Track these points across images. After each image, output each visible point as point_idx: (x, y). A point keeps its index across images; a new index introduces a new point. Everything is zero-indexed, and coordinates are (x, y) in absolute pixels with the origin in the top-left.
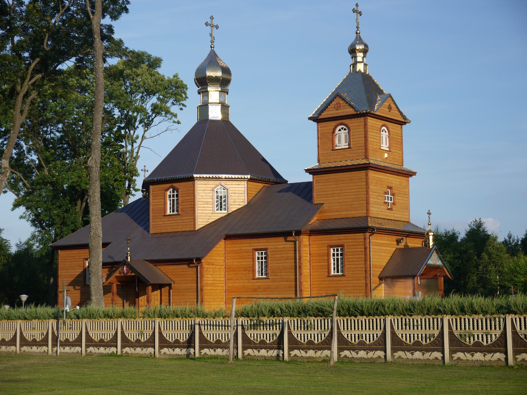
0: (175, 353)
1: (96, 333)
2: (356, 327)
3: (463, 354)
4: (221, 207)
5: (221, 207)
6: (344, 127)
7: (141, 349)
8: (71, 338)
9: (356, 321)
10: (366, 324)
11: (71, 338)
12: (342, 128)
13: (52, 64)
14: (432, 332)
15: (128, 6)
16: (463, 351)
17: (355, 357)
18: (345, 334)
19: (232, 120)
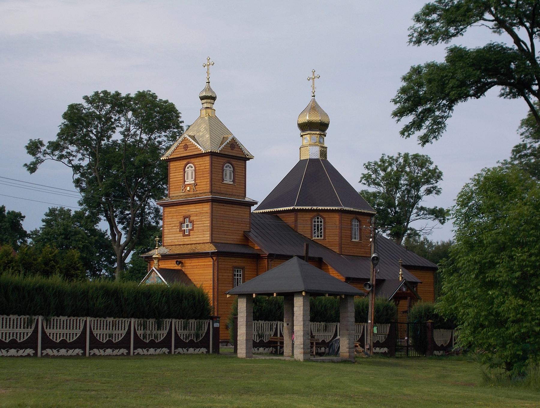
0: (149, 353)
1: (99, 330)
2: (68, 327)
3: (141, 350)
4: (318, 228)
5: (318, 228)
6: (231, 166)
7: (263, 349)
8: (101, 338)
9: (8, 320)
10: (17, 323)
11: (101, 338)
12: (228, 166)
13: (425, 93)
14: (75, 331)
15: (503, 97)
16: (51, 348)
17: (66, 355)
18: (95, 332)
19: (330, 159)
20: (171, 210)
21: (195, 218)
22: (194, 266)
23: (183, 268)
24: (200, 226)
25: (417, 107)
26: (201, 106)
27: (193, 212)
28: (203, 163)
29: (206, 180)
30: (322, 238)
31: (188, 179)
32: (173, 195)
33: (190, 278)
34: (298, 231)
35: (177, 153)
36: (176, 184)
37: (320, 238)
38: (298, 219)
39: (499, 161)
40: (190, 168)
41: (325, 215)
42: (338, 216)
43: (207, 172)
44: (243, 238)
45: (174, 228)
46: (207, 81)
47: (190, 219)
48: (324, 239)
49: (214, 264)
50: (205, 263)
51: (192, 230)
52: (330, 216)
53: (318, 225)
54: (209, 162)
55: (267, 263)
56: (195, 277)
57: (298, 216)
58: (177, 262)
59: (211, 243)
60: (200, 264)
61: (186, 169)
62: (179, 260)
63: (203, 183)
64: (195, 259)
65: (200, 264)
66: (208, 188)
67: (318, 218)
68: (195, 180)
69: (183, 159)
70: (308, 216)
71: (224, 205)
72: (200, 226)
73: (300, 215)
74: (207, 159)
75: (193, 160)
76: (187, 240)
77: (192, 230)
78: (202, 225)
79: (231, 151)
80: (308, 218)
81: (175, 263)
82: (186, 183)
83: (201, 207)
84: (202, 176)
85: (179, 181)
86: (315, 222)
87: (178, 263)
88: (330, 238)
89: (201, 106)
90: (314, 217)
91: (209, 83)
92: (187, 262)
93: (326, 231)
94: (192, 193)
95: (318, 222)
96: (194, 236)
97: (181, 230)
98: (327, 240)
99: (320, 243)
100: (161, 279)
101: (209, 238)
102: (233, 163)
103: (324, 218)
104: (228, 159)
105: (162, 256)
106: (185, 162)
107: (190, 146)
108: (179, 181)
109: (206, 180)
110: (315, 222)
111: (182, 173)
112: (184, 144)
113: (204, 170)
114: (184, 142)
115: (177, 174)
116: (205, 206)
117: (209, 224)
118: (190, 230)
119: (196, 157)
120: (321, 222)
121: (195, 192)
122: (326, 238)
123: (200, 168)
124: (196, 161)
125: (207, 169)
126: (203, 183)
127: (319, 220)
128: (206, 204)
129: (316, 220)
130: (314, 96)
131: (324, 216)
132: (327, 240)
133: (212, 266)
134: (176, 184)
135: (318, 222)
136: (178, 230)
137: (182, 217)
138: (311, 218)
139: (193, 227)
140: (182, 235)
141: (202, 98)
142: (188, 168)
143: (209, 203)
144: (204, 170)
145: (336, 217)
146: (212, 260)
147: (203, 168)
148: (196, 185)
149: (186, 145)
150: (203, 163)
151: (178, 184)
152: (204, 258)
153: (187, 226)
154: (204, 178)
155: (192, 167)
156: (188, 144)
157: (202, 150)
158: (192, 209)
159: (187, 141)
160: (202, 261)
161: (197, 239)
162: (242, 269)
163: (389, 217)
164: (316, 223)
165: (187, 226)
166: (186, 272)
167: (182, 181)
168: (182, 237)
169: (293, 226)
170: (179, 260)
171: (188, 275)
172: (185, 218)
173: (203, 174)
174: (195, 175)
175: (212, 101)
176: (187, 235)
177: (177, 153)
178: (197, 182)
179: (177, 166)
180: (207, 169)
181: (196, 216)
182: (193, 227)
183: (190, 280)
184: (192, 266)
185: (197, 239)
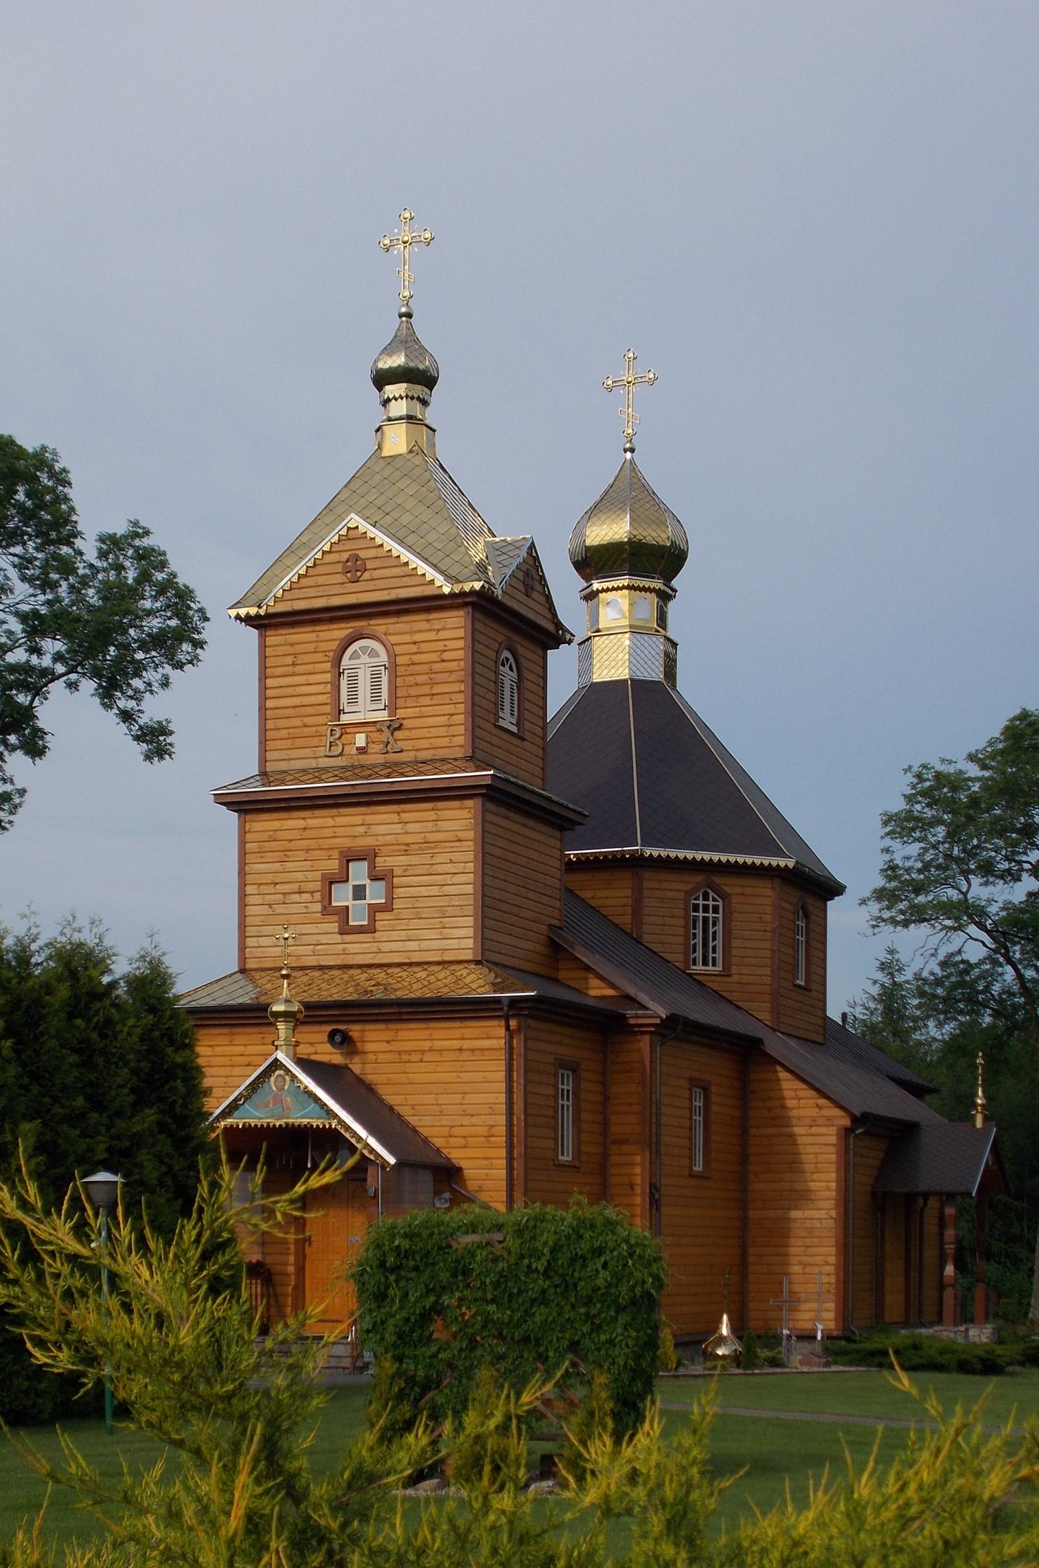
4: (705, 930)
5: (705, 930)
20: (276, 824)
21: (402, 860)
22: (409, 1052)
23: (357, 1059)
24: (424, 891)
25: (181, 644)
26: (380, 415)
27: (389, 839)
28: (431, 636)
29: (450, 709)
30: (719, 968)
31: (353, 700)
32: (284, 766)
33: (391, 1099)
34: (646, 938)
35: (312, 592)
36: (297, 722)
37: (710, 968)
38: (646, 893)
39: (910, 767)
40: (365, 659)
41: (731, 885)
42: (769, 892)
43: (454, 677)
44: (539, 948)
45: (296, 897)
46: (404, 310)
47: (372, 867)
48: (726, 973)
49: (510, 1049)
50: (466, 1044)
51: (388, 907)
52: (747, 891)
53: (705, 920)
54: (461, 633)
55: (648, 1049)
56: (412, 1099)
57: (645, 884)
58: (332, 1035)
59: (478, 963)
60: (438, 1044)
61: (346, 661)
62: (342, 1027)
63: (431, 721)
64: (413, 1025)
65: (438, 1044)
66: (460, 740)
67: (706, 897)
68: (392, 707)
69: (332, 620)
70: (677, 885)
71: (511, 815)
72: (424, 891)
73: (651, 880)
74: (455, 625)
75: (379, 625)
76: (359, 950)
77: (388, 907)
78: (434, 891)
79: (522, 597)
80: (676, 895)
81: (325, 1037)
82: (345, 719)
83: (432, 815)
84: (426, 690)
85: (311, 710)
86: (696, 908)
87: (338, 1038)
88: (745, 970)
89: (380, 415)
90: (697, 889)
91: (409, 315)
92: (370, 1036)
93: (735, 943)
94: (375, 758)
95: (706, 908)
96: (395, 935)
97: (328, 909)
98: (735, 978)
99: (715, 986)
100: (317, 1099)
101: (470, 943)
102: (521, 650)
103: (724, 896)
104: (510, 634)
105: (308, 1006)
106: (340, 631)
107: (377, 564)
108: (311, 710)
109: (450, 709)
110: (696, 908)
111: (327, 677)
112: (345, 556)
113: (437, 667)
114: (349, 545)
115: (302, 679)
116: (449, 814)
117: (470, 889)
118: (374, 910)
119: (398, 613)
120: (716, 910)
121: (392, 757)
122: (734, 970)
123: (416, 658)
124: (396, 628)
125: (454, 665)
126: (431, 721)
127: (711, 903)
128: (457, 803)
129: (701, 902)
130: (632, 450)
131: (728, 889)
132: (735, 978)
133: (502, 1055)
134: (297, 722)
135: (706, 908)
136: (318, 907)
137: (336, 854)
138: (686, 892)
139: (390, 897)
140: (334, 927)
141: (382, 379)
142: (355, 656)
143: (470, 803)
144: (437, 667)
145: (765, 894)
146: (502, 1032)
147: (434, 657)
148: (400, 728)
149: (357, 558)
150: (431, 636)
151: (307, 720)
152: (457, 1024)
153: (359, 892)
154: (436, 700)
155: (372, 653)
156: (362, 554)
157: (439, 580)
158: (418, 820)
159: (361, 543)
160: (448, 1033)
161: (413, 945)
162: (574, 1071)
163: (55, 963)
164: (701, 914)
165: (359, 892)
166: (370, 1078)
167: (328, 709)
168: (338, 938)
169: (625, 920)
170: (342, 1027)
171: (380, 1090)
172: (349, 857)
173: (433, 684)
174: (393, 688)
175: (419, 390)
176: (360, 930)
177: (312, 592)
178: (400, 713)
179: (298, 649)
180: (454, 665)
181: (406, 853)
182: (390, 897)
183: (391, 1108)
184: (399, 1053)
185: (413, 945)
